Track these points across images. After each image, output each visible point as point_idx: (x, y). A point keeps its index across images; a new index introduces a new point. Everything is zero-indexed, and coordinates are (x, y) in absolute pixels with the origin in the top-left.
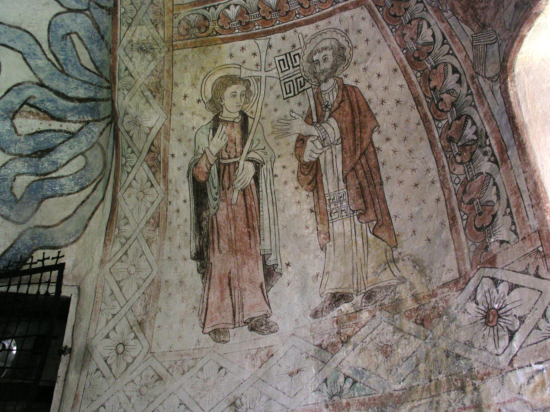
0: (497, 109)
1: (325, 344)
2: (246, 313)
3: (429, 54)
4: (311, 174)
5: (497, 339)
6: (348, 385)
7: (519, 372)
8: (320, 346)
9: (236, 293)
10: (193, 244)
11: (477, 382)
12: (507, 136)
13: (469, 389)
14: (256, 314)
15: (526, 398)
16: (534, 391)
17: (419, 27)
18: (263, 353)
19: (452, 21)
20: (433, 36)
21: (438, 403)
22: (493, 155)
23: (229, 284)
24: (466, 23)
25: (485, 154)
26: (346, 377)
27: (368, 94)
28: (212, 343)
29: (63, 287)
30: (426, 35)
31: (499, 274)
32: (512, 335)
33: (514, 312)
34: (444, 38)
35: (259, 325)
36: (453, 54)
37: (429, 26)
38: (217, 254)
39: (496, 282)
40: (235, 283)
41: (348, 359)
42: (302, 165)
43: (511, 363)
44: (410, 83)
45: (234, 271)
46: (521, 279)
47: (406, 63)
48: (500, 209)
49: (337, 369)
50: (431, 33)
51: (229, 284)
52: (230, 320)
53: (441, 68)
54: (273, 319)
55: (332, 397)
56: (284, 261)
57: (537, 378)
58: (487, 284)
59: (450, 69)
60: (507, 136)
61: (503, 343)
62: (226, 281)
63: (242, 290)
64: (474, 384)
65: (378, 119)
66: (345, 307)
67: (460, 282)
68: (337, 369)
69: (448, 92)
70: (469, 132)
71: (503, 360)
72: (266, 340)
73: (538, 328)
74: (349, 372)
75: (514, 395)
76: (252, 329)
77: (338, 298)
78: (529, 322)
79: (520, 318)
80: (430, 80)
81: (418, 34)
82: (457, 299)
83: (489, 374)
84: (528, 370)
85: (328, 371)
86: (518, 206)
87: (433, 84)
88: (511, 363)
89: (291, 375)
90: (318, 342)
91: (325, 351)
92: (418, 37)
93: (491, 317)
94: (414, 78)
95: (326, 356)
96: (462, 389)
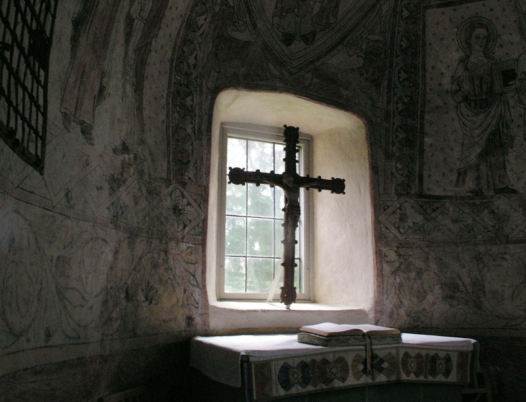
0: (205, 107)
1: (116, 176)
3: (194, 31)
4: (130, 21)
5: (179, 225)
7: (184, 244)
10: (78, 8)
11: (168, 240)
12: (204, 127)
13: (164, 241)
15: (183, 255)
16: (187, 254)
17: (203, 14)
19: (211, 31)
20: (202, 25)
21: (151, 242)
22: (194, 128)
24: (213, 42)
25: (191, 123)
27: (167, 12)
30: (201, 21)
31: (186, 193)
32: (185, 226)
33: (188, 216)
34: (203, 34)
36: (200, 47)
37: (205, 20)
39: (183, 197)
41: (124, 196)
42: (129, 13)
43: (183, 238)
44: (179, 33)
46: (192, 202)
47: (186, 20)
48: (192, 159)
50: (202, 23)
53: (192, 46)
57: (189, 250)
58: (178, 193)
59: (195, 54)
60: (204, 127)
61: (181, 227)
64: (166, 241)
65: (160, 32)
67: (168, 182)
69: (188, 64)
70: (188, 102)
71: (180, 235)
73: (194, 229)
75: (179, 252)
76: (83, 132)
77: (125, 149)
78: (194, 224)
79: (190, 220)
80: (185, 45)
81: (200, 15)
82: (165, 191)
83: (173, 239)
84: (188, 244)
86: (200, 169)
87: (185, 48)
88: (183, 238)
89: (97, 188)
90: (112, 172)
92: (198, 16)
93: (176, 210)
94: (181, 32)
96: (161, 240)
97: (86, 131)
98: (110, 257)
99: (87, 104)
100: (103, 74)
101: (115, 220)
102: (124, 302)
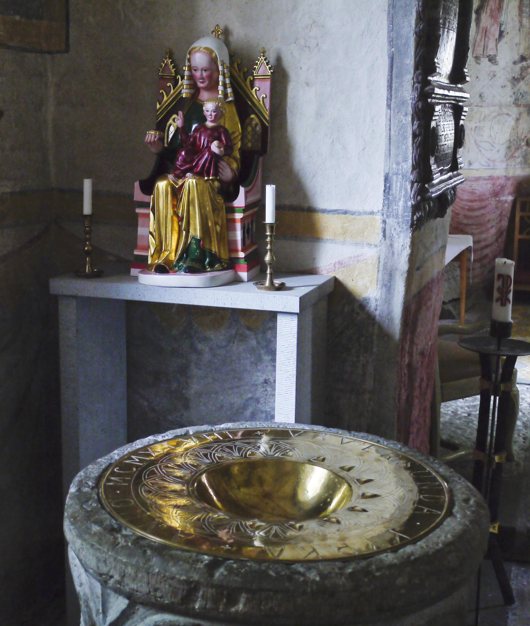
1: (516, 77)
2: (488, 51)
6: (521, 96)
8: (514, 78)
9: (486, 40)
14: (492, 53)
18: (492, 74)
23: (485, 34)
26: (521, 94)
28: (475, 63)
29: (454, 128)
35: (492, 59)
38: (484, 14)
40: (488, 33)
45: (489, 27)
49: (519, 90)
51: (485, 34)
52: (482, 53)
54: (497, 58)
55: (515, 100)
56: (507, 31)
62: (484, 31)
63: (489, 39)
66: (524, 63)
68: (519, 90)
72: (494, 68)
74: (522, 92)
76: (490, 60)
85: (516, 89)
89: (502, 87)
90: (513, 76)
91: (515, 80)
95: (516, 83)
97: (492, 59)
98: (513, 123)
99: (491, 44)
100: (501, 25)
101: (516, 103)
102: (525, 148)
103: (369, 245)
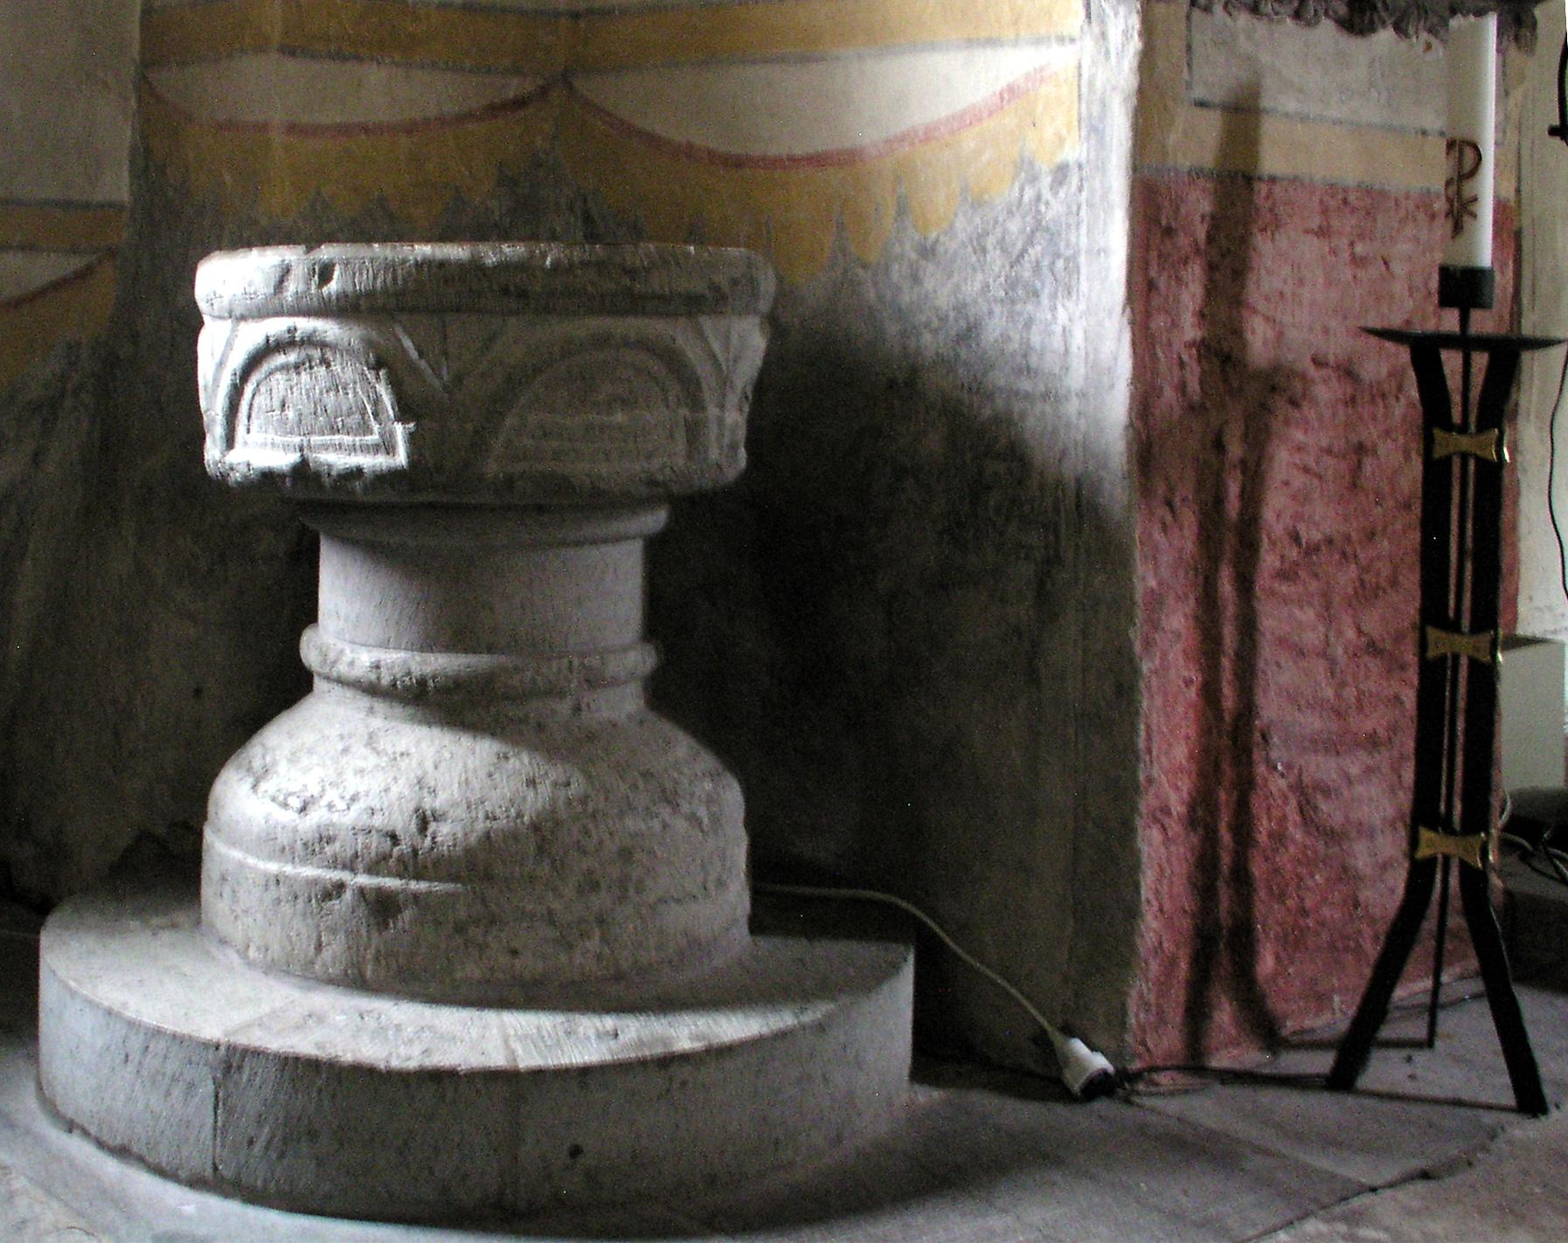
103: (1061, 40)
